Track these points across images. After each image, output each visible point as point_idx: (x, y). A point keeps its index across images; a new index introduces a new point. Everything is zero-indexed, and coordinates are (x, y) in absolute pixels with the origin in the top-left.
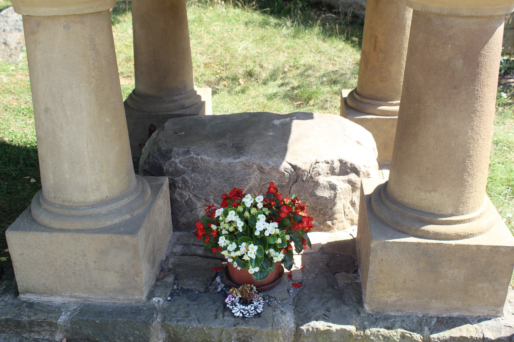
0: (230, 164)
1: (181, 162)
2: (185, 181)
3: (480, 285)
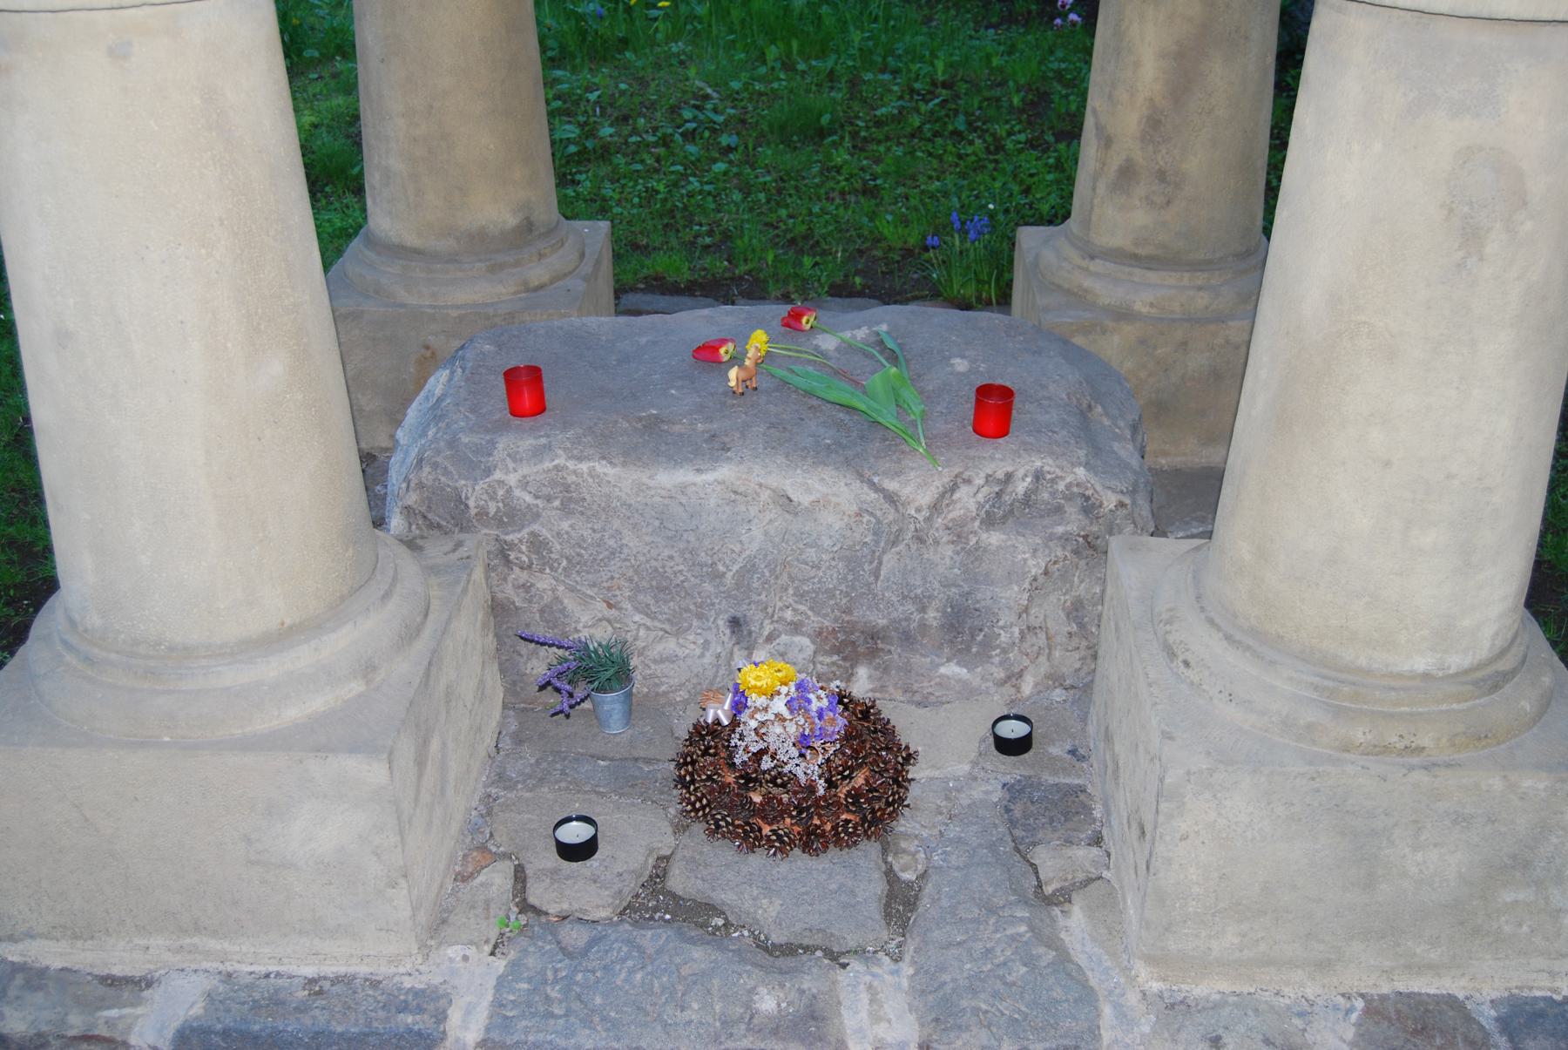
0: (683, 488)
1: (524, 484)
2: (537, 544)
3: (1508, 896)
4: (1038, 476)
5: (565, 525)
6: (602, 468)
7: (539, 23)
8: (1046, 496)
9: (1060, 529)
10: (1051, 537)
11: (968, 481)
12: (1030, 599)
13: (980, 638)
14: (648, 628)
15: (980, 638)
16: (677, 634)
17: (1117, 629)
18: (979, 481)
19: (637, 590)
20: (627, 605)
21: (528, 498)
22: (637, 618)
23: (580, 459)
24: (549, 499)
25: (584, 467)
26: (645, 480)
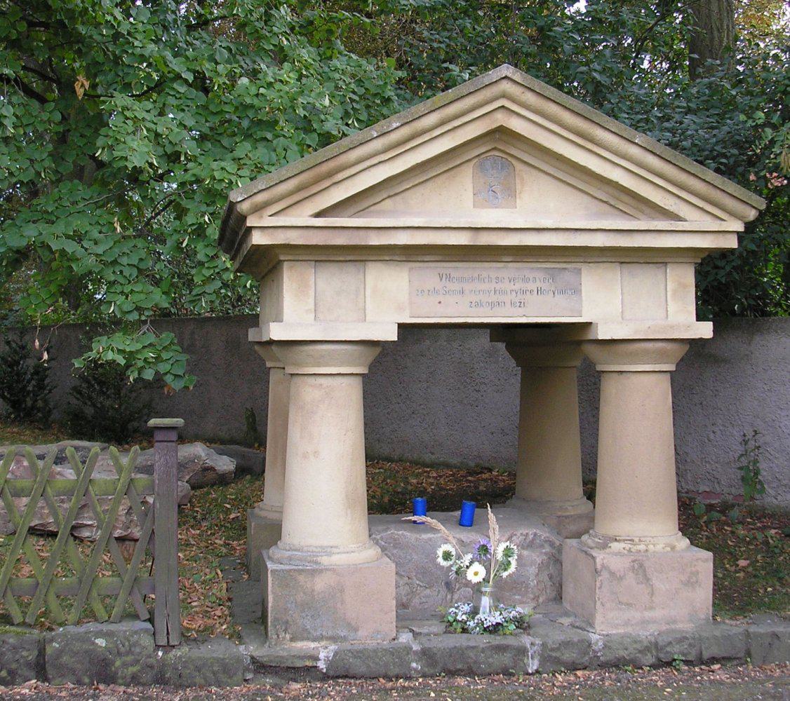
0: (430, 539)
4: (535, 535)
5: (395, 551)
6: (405, 533)
7: (715, 576)
8: (538, 541)
9: (544, 551)
10: (541, 553)
11: (516, 535)
12: (539, 571)
13: (524, 585)
14: (421, 586)
15: (524, 585)
16: (430, 588)
17: (437, 267)
18: (519, 535)
19: (417, 573)
20: (414, 578)
21: (383, 543)
22: (418, 582)
23: (398, 530)
24: (390, 543)
25: (401, 532)
26: (418, 536)
